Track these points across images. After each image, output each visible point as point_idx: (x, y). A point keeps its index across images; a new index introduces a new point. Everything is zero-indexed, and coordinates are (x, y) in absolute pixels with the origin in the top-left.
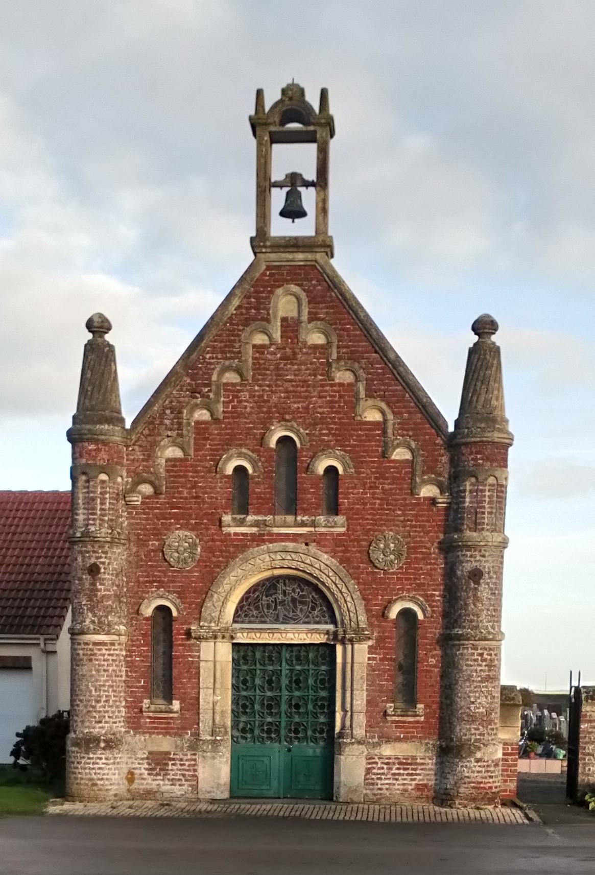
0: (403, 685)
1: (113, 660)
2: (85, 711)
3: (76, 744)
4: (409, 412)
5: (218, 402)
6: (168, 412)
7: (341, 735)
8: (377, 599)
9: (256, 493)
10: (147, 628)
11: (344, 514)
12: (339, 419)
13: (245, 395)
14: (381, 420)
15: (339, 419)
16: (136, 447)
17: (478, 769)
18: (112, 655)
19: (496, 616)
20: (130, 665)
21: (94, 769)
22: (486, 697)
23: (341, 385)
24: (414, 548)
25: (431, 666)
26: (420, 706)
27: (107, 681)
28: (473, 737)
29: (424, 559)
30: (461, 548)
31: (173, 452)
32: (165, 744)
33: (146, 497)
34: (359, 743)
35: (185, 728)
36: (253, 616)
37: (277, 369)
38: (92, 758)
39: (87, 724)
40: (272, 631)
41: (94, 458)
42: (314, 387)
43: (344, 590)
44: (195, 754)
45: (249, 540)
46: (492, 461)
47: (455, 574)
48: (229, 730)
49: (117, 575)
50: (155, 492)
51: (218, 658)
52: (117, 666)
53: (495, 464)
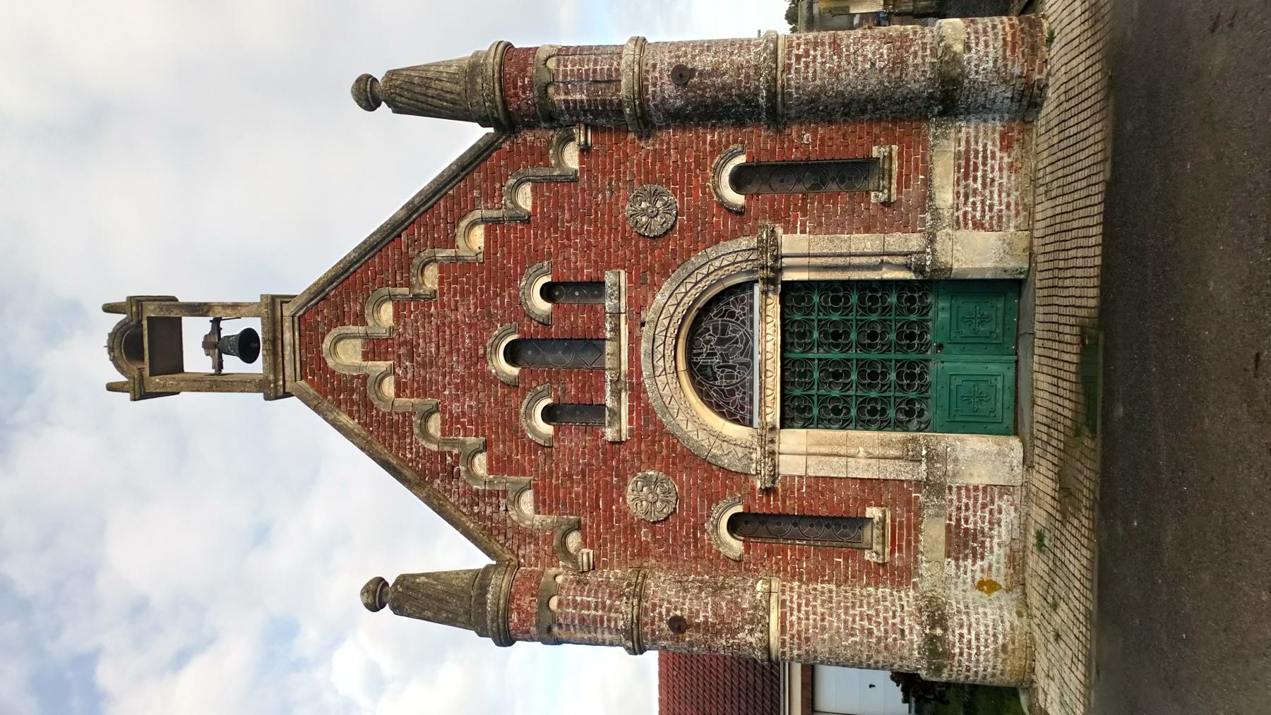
0: (842, 181)
1: (807, 605)
2: (886, 654)
3: (939, 670)
4: (473, 188)
5: (464, 443)
6: (476, 509)
7: (920, 269)
8: (718, 222)
9: (577, 393)
10: (759, 549)
11: (603, 274)
12: (482, 283)
13: (455, 408)
14: (483, 226)
15: (482, 283)
16: (521, 552)
17: (981, 47)
18: (799, 605)
19: (744, 45)
20: (814, 576)
21: (978, 648)
22: (864, 45)
23: (441, 281)
24: (647, 173)
25: (814, 141)
26: (875, 152)
27: (838, 615)
28: (928, 60)
29: (662, 161)
30: (643, 103)
31: (527, 502)
32: (933, 533)
33: (584, 543)
34: (932, 241)
35: (909, 502)
36: (743, 399)
37: (423, 365)
38: (961, 649)
39: (906, 652)
40: (763, 372)
41: (529, 614)
42: (445, 317)
43: (705, 271)
44: (950, 488)
45: (639, 404)
46: (526, 64)
47: (682, 109)
48: (909, 435)
49: (686, 590)
50: (579, 529)
51: (803, 449)
52: (815, 599)
53: (530, 60)
